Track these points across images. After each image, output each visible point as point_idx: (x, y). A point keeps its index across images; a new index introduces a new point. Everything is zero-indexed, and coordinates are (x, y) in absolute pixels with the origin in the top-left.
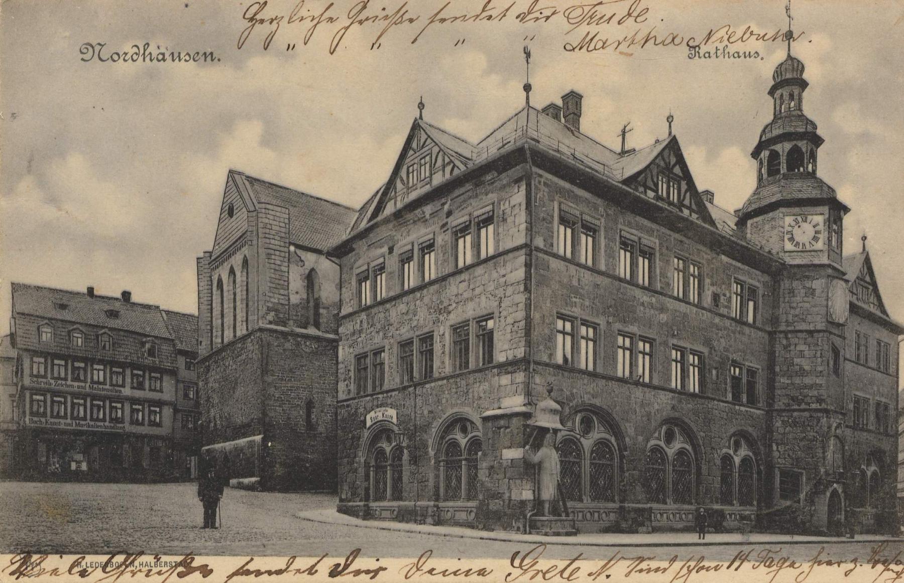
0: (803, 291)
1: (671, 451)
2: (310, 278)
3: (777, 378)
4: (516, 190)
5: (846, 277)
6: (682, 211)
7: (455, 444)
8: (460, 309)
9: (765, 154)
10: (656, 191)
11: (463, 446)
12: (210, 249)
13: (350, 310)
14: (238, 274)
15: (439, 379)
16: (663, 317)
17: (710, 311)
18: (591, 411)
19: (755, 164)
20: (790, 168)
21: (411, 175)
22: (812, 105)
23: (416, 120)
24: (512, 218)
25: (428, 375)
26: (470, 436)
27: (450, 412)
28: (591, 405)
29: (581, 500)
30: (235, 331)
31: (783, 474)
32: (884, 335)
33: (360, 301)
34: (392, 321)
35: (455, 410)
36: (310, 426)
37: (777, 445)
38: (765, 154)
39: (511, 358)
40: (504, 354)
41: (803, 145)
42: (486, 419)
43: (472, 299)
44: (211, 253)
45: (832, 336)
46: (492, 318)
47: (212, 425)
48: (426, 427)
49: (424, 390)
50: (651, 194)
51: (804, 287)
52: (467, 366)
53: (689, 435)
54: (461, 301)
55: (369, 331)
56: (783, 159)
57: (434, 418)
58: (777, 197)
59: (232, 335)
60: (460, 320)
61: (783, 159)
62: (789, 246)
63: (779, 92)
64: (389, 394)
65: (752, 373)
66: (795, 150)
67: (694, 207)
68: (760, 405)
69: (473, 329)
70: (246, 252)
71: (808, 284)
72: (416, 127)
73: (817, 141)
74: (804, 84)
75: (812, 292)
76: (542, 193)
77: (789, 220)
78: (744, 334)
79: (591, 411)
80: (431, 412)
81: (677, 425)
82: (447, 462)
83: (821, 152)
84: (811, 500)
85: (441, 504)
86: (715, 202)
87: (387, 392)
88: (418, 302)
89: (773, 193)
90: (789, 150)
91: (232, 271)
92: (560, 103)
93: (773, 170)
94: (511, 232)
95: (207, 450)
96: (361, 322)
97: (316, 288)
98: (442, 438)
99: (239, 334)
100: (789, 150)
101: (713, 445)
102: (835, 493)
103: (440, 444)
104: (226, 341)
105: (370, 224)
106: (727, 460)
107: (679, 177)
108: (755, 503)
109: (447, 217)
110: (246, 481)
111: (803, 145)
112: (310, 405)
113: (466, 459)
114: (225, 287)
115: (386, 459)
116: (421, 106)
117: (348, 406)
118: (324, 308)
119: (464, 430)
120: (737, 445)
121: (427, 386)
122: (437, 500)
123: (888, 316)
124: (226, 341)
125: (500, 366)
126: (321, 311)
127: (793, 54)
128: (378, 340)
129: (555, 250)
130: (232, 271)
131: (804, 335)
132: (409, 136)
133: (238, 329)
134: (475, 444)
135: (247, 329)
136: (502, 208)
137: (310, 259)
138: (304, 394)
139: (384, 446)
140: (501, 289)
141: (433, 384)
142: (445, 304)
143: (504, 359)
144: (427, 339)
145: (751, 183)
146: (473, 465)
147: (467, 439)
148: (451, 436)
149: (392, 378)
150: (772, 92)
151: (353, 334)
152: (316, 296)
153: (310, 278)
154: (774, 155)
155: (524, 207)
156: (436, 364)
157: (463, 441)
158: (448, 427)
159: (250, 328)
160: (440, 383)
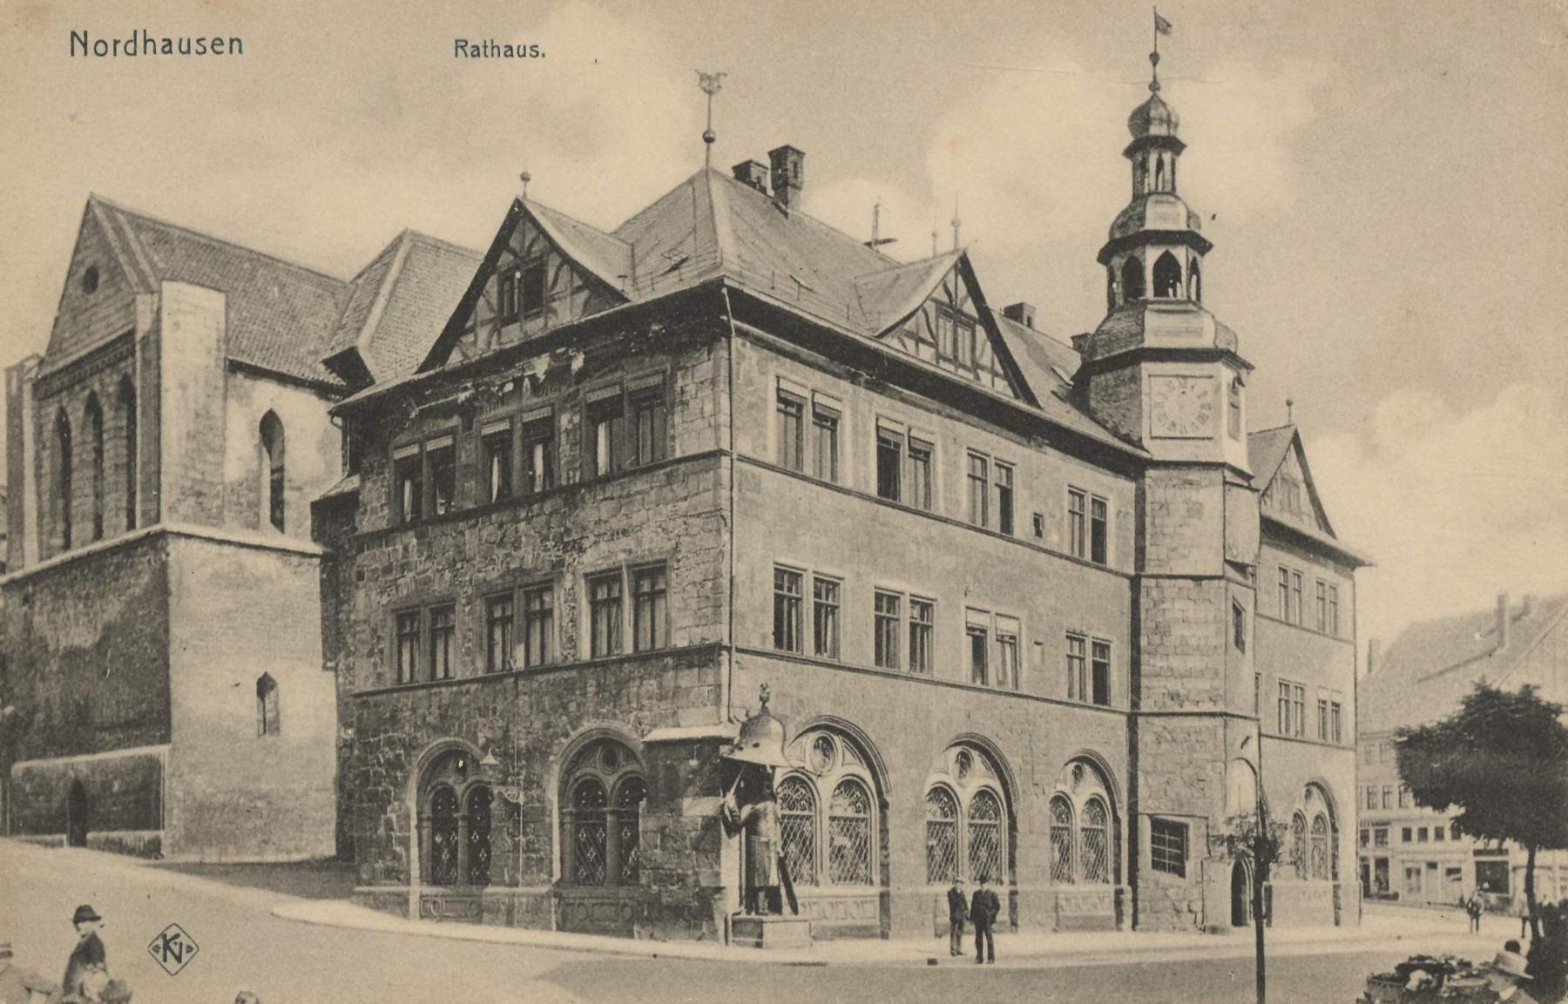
2: (270, 428)
4: (705, 356)
5: (1253, 483)
6: (978, 378)
7: (593, 785)
8: (603, 546)
9: (1118, 262)
10: (935, 345)
14: (108, 414)
17: (1030, 546)
18: (827, 727)
19: (1103, 270)
20: (1160, 290)
27: (587, 725)
28: (831, 719)
31: (1158, 825)
32: (1327, 573)
34: (469, 553)
38: (1118, 262)
39: (696, 642)
40: (683, 633)
41: (1181, 254)
43: (625, 532)
45: (1232, 586)
47: (40, 716)
49: (535, 685)
50: (926, 353)
51: (1186, 502)
53: (997, 765)
55: (421, 568)
60: (604, 565)
64: (464, 688)
65: (1102, 648)
67: (998, 368)
73: (1201, 246)
74: (1175, 146)
75: (1195, 510)
79: (827, 727)
81: (976, 747)
83: (1206, 263)
86: (1036, 322)
88: (522, 526)
90: (1147, 259)
91: (93, 406)
95: (28, 771)
96: (406, 549)
101: (1038, 777)
105: (423, 375)
106: (1061, 801)
107: (970, 317)
109: (577, 383)
110: (128, 836)
111: (1181, 254)
113: (612, 813)
116: (525, 178)
117: (377, 705)
118: (293, 489)
119: (610, 761)
120: (1078, 774)
123: (1330, 532)
132: (858, 937)
136: (680, 383)
137: (266, 395)
139: (450, 781)
140: (680, 521)
142: (575, 536)
143: (686, 644)
146: (628, 819)
147: (615, 777)
148: (587, 770)
151: (388, 570)
153: (270, 428)
157: (610, 781)
158: (580, 754)
160: (566, 675)
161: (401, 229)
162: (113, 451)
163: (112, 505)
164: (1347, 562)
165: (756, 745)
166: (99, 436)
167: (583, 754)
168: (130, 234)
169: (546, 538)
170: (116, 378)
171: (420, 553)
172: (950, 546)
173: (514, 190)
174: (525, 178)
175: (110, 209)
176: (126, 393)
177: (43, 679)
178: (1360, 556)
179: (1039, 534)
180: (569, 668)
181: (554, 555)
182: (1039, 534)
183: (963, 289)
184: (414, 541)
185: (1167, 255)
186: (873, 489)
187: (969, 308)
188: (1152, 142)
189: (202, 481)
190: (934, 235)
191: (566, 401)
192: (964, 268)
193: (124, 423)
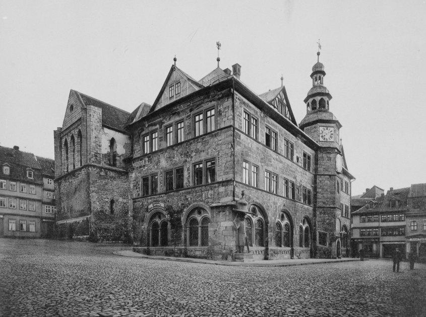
0: (327, 159)
1: (283, 224)
2: (112, 142)
3: (318, 194)
4: (226, 100)
9: (310, 100)
11: (199, 221)
12: (61, 127)
13: (139, 156)
14: (76, 139)
15: (186, 189)
16: (281, 165)
21: (177, 89)
22: (328, 83)
23: (173, 66)
24: (224, 113)
25: (180, 186)
26: (202, 216)
29: (281, 246)
30: (74, 166)
33: (144, 152)
35: (195, 203)
36: (112, 212)
37: (318, 222)
41: (326, 98)
42: (212, 208)
44: (61, 129)
46: (202, 163)
47: (62, 210)
48: (181, 211)
52: (201, 183)
54: (198, 151)
56: (318, 103)
57: (184, 207)
58: (317, 119)
59: (72, 168)
61: (318, 103)
62: (321, 139)
63: (315, 75)
66: (322, 100)
68: (312, 205)
69: (150, 178)
70: (80, 128)
71: (329, 155)
72: (173, 69)
74: (324, 73)
75: (330, 159)
76: (237, 104)
77: (321, 128)
78: (306, 175)
80: (182, 204)
82: (202, 227)
84: (330, 244)
85: (187, 248)
87: (159, 194)
89: (314, 117)
90: (318, 100)
91: (73, 138)
92: (231, 69)
93: (314, 108)
94: (224, 120)
97: (115, 147)
98: (188, 216)
99: (76, 167)
100: (318, 100)
102: (338, 242)
103: (187, 220)
104: (69, 171)
106: (301, 227)
108: (310, 246)
112: (112, 202)
113: (200, 227)
114: (69, 145)
115: (197, 223)
116: (175, 60)
119: (160, 217)
121: (180, 192)
122: (148, 246)
123: (347, 169)
124: (69, 171)
125: (219, 183)
126: (117, 158)
127: (320, 62)
128: (154, 171)
129: (242, 131)
130: (73, 138)
131: (328, 177)
133: (83, 162)
134: (206, 220)
135: (81, 165)
138: (110, 197)
139: (157, 220)
141: (184, 191)
144: (180, 171)
145: (305, 114)
149: (161, 188)
150: (312, 76)
151: (141, 167)
152: (114, 151)
154: (314, 102)
155: (230, 108)
156: (185, 181)
158: (192, 211)
159: (83, 165)
161: (142, 102)
162: (77, 147)
163: (77, 160)
164: (351, 177)
165: (341, 140)
166: (74, 145)
167: (192, 212)
168: (80, 97)
169: (182, 155)
170: (77, 130)
171: (149, 162)
172: (281, 162)
173: (173, 63)
174: (175, 60)
175: (76, 92)
176: (80, 135)
177: (63, 202)
178: (354, 176)
179: (298, 162)
180: (189, 189)
181: (184, 159)
182: (298, 162)
183: (283, 97)
184: (147, 159)
185: (322, 99)
186: (265, 144)
187: (285, 101)
188: (318, 72)
189: (97, 153)
190: (282, 79)
191: (187, 117)
192: (284, 90)
193: (79, 141)
